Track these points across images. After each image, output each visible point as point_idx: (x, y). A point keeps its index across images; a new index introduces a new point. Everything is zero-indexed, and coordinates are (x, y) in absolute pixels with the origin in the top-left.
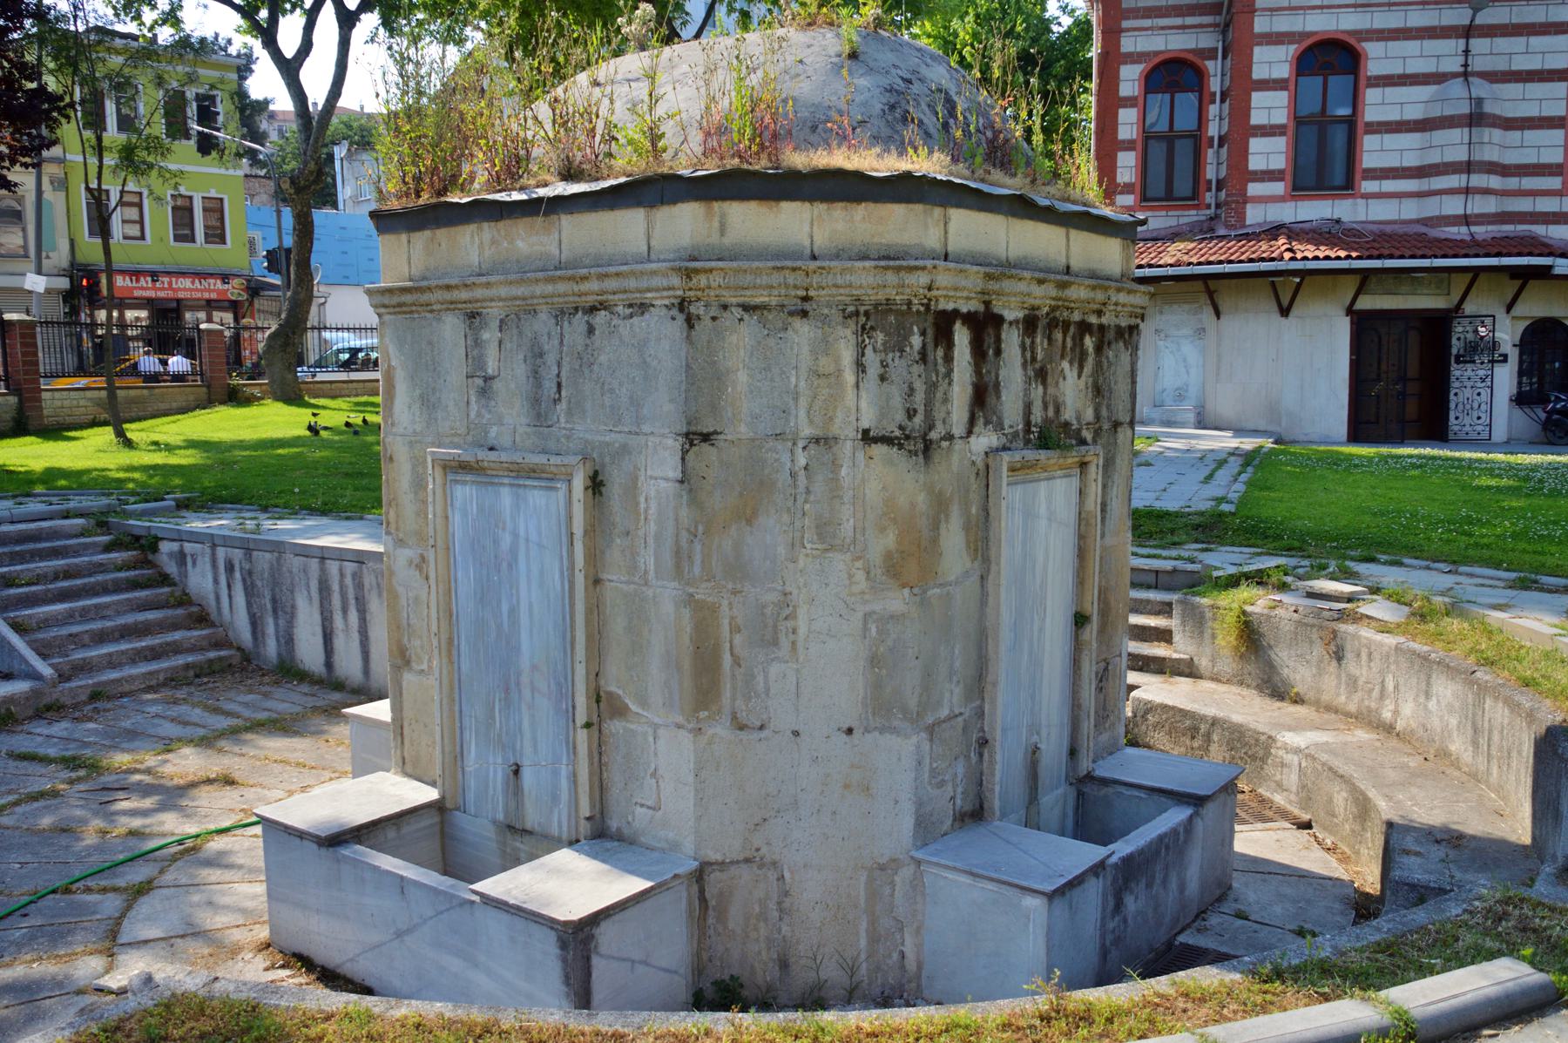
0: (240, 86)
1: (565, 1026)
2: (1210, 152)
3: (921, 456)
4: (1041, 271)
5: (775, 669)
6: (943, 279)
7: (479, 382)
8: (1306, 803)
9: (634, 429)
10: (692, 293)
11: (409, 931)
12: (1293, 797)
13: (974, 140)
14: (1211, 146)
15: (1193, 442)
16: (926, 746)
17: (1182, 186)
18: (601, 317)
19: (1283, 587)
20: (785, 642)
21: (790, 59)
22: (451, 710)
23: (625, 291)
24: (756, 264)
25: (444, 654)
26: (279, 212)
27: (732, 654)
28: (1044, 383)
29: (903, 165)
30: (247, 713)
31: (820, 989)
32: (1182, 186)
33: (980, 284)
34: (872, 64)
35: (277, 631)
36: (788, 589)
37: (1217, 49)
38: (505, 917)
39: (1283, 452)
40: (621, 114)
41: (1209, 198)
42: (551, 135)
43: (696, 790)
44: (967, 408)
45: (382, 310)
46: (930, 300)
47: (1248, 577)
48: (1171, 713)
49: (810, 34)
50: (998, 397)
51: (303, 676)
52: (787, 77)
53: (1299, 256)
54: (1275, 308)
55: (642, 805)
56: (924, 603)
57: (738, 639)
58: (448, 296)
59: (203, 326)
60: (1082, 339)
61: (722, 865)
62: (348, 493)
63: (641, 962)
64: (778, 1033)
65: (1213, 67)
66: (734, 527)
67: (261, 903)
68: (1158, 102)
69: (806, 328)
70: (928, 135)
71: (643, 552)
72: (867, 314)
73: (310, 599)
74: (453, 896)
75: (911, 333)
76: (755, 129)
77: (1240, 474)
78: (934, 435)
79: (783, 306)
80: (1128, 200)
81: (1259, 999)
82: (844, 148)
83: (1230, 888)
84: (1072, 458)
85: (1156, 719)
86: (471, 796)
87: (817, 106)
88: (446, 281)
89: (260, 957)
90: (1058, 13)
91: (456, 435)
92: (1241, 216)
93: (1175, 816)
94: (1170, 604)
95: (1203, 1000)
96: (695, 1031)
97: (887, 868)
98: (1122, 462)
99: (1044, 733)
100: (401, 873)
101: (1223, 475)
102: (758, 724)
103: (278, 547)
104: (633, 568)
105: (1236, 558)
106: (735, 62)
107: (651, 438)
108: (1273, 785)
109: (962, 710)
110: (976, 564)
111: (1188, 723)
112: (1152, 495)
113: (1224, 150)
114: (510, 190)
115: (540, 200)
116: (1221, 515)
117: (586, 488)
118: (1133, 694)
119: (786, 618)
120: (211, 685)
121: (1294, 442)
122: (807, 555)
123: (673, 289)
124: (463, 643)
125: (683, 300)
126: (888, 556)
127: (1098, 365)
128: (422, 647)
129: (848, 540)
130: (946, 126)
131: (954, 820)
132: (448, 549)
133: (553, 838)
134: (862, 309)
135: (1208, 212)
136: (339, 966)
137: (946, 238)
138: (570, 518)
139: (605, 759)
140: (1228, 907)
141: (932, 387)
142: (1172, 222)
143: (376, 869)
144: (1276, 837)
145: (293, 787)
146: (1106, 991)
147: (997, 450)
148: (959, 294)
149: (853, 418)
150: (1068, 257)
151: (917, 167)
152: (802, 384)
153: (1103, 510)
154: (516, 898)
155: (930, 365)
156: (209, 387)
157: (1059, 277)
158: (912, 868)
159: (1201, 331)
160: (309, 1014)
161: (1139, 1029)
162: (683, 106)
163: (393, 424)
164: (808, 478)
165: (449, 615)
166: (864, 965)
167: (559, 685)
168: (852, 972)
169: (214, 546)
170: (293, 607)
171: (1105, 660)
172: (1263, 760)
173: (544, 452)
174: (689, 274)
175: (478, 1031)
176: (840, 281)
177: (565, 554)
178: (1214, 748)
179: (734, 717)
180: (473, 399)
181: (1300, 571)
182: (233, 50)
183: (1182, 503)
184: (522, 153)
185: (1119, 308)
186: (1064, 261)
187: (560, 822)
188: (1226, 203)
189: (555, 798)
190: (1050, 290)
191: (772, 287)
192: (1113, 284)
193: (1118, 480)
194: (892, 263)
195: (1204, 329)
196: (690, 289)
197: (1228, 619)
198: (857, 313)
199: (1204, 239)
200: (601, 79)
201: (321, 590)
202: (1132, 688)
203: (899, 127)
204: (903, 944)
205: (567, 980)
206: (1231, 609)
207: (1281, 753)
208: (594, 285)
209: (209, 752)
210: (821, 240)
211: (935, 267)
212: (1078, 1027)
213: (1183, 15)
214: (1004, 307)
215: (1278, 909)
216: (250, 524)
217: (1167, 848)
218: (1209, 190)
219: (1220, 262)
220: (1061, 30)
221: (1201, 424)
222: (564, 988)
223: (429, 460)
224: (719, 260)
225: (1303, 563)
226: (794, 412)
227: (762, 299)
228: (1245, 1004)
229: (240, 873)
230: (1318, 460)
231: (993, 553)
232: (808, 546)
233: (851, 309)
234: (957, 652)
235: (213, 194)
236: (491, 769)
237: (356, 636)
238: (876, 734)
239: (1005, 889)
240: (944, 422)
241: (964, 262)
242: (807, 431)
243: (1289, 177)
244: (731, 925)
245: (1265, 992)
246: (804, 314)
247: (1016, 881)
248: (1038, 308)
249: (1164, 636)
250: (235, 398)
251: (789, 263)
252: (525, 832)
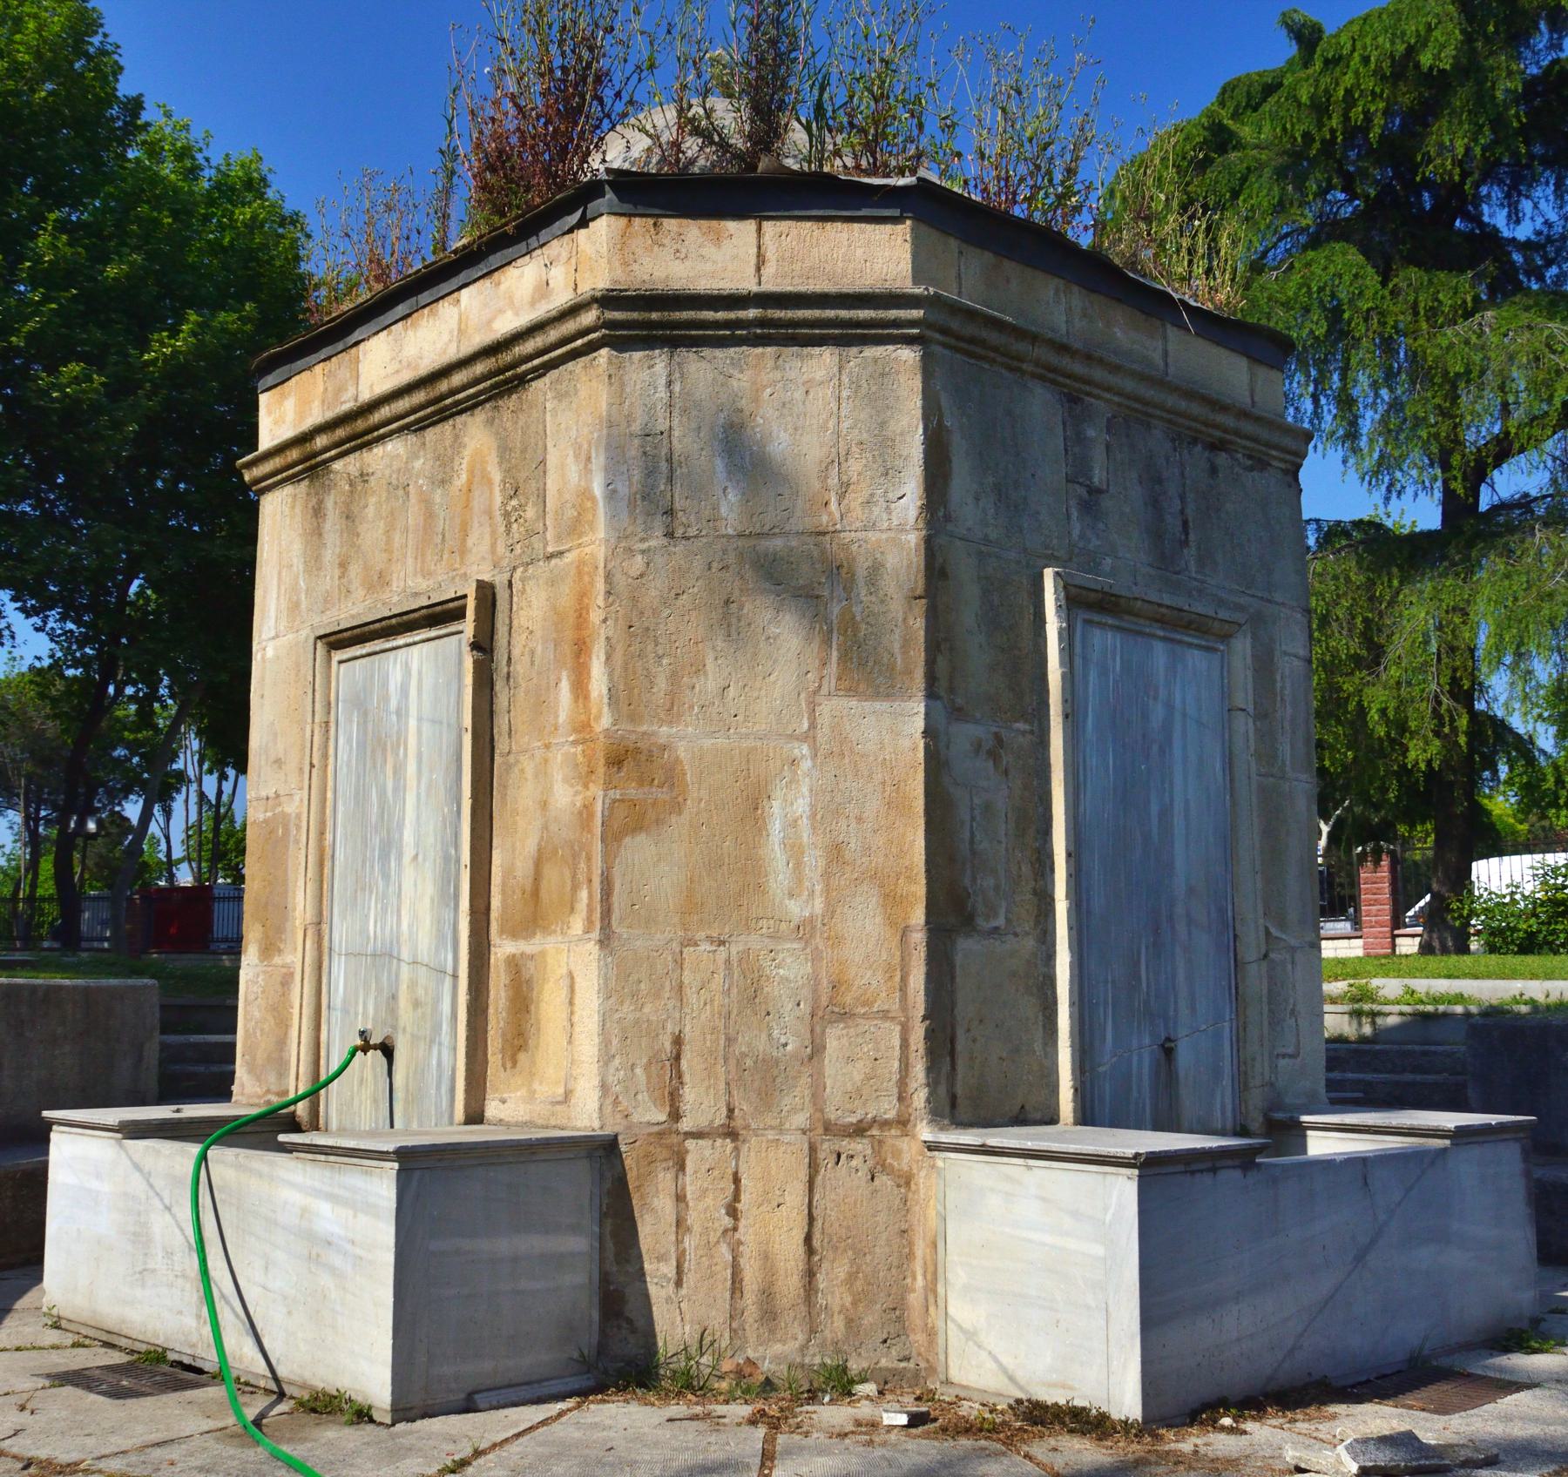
7: (1082, 491)
55: (1284, 1056)
128: (997, 888)
236: (1135, 1059)
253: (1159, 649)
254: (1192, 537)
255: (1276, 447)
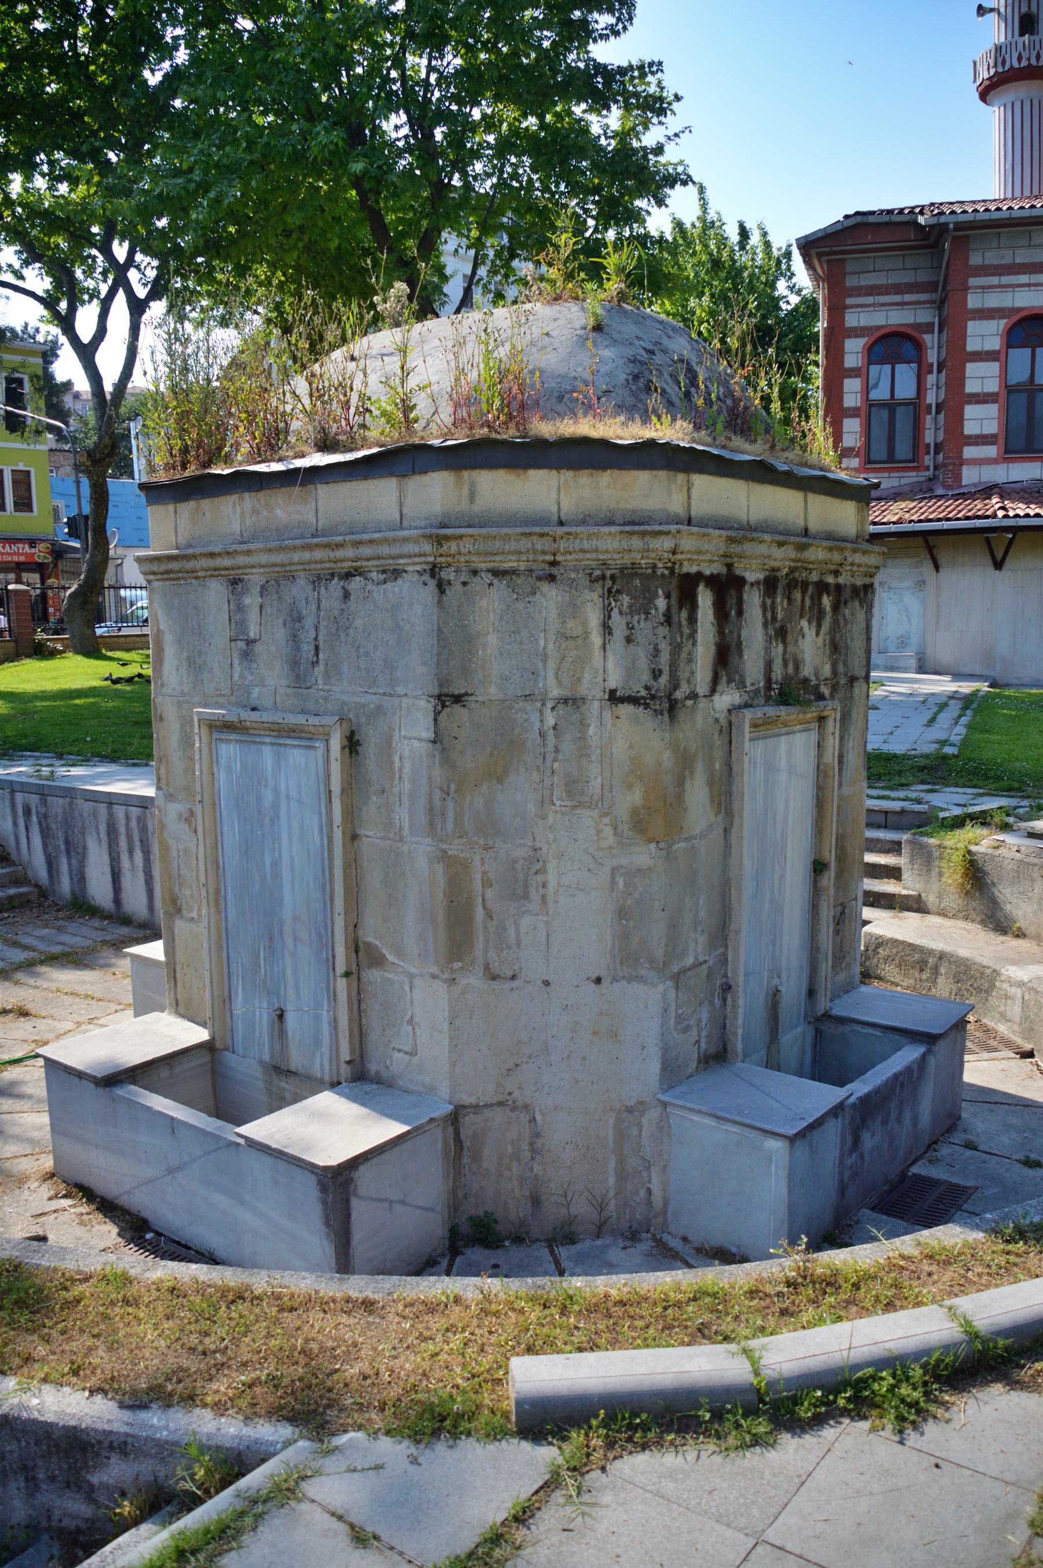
0: (45, 370)
1: (317, 1292)
2: (928, 418)
3: (666, 715)
4: (780, 533)
5: (526, 922)
6: (687, 543)
7: (242, 645)
8: (1028, 1033)
9: (389, 690)
10: (443, 559)
11: (179, 1169)
12: (1016, 1027)
13: (715, 408)
14: (930, 413)
15: (916, 686)
16: (672, 994)
17: (903, 450)
18: (356, 583)
19: (1005, 827)
20: (535, 897)
21: (536, 331)
22: (219, 957)
23: (379, 558)
24: (504, 531)
25: (212, 904)
26: (78, 483)
27: (484, 908)
28: (784, 643)
29: (648, 433)
30: (42, 946)
31: (570, 1224)
32: (903, 450)
33: (722, 548)
34: (616, 336)
35: (70, 871)
36: (538, 845)
37: (933, 324)
38: (268, 1159)
39: (999, 696)
40: (375, 387)
41: (928, 460)
42: (308, 407)
43: (451, 1038)
44: (710, 667)
45: (152, 577)
46: (674, 563)
47: (972, 817)
48: (901, 948)
49: (556, 308)
50: (741, 656)
51: (92, 911)
52: (534, 350)
53: (1011, 513)
54: (989, 561)
56: (669, 857)
57: (490, 893)
58: (211, 563)
59: (11, 587)
60: (820, 598)
61: (476, 1108)
62: (136, 741)
63: (398, 1202)
64: (526, 1302)
65: (930, 340)
66: (485, 786)
67: (46, 1134)
68: (880, 373)
69: (554, 593)
70: (670, 403)
71: (397, 809)
72: (613, 578)
73: (100, 841)
74: (219, 1138)
75: (657, 596)
76: (503, 399)
77: (960, 717)
78: (678, 695)
79: (531, 571)
80: (855, 462)
81: (1002, 1260)
82: (590, 417)
83: (959, 1118)
84: (811, 714)
85: (887, 952)
86: (239, 1037)
87: (564, 377)
88: (211, 549)
89: (45, 1186)
90: (786, 292)
91: (221, 695)
92: (958, 477)
93: (909, 1055)
94: (899, 843)
95: (947, 1263)
96: (444, 1299)
97: (635, 1110)
98: (856, 715)
99: (784, 976)
100: (171, 1114)
101: (945, 718)
102: (510, 974)
103: (70, 793)
104: (388, 824)
105: (961, 799)
106: (483, 334)
107: (404, 700)
108: (997, 1015)
109: (707, 958)
110: (720, 818)
111: (917, 956)
112: (881, 738)
113: (941, 417)
114: (269, 461)
115: (297, 470)
116: (945, 758)
117: (343, 748)
118: (866, 929)
119: (536, 873)
120: (11, 920)
121: (1008, 685)
122: (556, 812)
123: (425, 555)
124: (229, 895)
125: (434, 566)
126: (635, 812)
127: (835, 626)
128: (192, 896)
129: (596, 797)
130: (687, 395)
131: (699, 1062)
132: (214, 804)
133: (316, 1079)
134: (608, 573)
135: (927, 473)
136: (116, 1198)
137: (689, 504)
138: (328, 775)
139: (363, 1006)
140: (958, 1137)
141: (676, 649)
142: (895, 483)
143: (148, 1109)
144: (1001, 1067)
145: (81, 1019)
146: (851, 1253)
147: (740, 707)
148: (702, 558)
149: (600, 679)
150: (806, 520)
151: (660, 434)
152: (551, 646)
153: (841, 762)
154: (278, 1143)
155: (675, 627)
156: (16, 642)
157: (798, 539)
158: (659, 1109)
159: (921, 584)
160: (68, 1275)
161: (886, 1297)
162: (434, 379)
163: (162, 685)
164: (557, 736)
165: (216, 866)
166: (613, 1202)
167: (319, 934)
168: (601, 1207)
169: (13, 792)
170: (85, 848)
171: (842, 904)
172: (988, 992)
173: (303, 712)
174: (439, 540)
175: (230, 1297)
176: (586, 546)
177: (323, 810)
178: (941, 980)
179: (487, 968)
180: (236, 662)
181: (1021, 811)
182: (40, 338)
183: (908, 746)
184: (282, 425)
185: (855, 568)
186: (802, 523)
187: (322, 1065)
188: (944, 465)
189: (317, 1042)
190: (790, 552)
191: (521, 553)
192: (849, 545)
193: (854, 732)
194: (636, 528)
195: (924, 582)
196: (441, 556)
197: (954, 858)
198: (603, 577)
199: (924, 498)
200: (356, 354)
201: (109, 833)
202: (866, 923)
203: (643, 396)
204: (650, 1181)
205: (327, 1222)
206: (957, 849)
207: (1005, 986)
208: (349, 552)
209: (7, 984)
210: (568, 506)
211: (679, 532)
212: (825, 1293)
213: (902, 293)
214: (745, 569)
215: (1005, 1139)
216: (46, 771)
217: (902, 1084)
218: (928, 453)
219: (939, 520)
220: (789, 308)
221: (922, 669)
222: (324, 1229)
223: (196, 719)
224: (469, 526)
225: (1022, 804)
226: (542, 673)
227: (511, 564)
228: (989, 1266)
229: (30, 1103)
230: (1032, 703)
231: (736, 806)
232: (558, 803)
233: (598, 573)
234: (701, 902)
235: (21, 467)
237: (141, 875)
238: (624, 982)
239: (747, 1132)
240: (688, 681)
241: (706, 526)
242: (555, 692)
243: (1001, 441)
244: (485, 1165)
245: (1008, 1253)
246: (552, 578)
247: (758, 1124)
248: (778, 569)
249: (894, 873)
250: (41, 652)
251: (537, 529)
252: (290, 1073)
253: (267, 750)
254: (321, 656)
255: (401, 556)
